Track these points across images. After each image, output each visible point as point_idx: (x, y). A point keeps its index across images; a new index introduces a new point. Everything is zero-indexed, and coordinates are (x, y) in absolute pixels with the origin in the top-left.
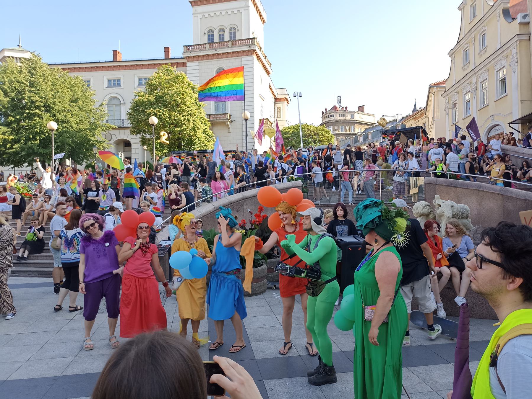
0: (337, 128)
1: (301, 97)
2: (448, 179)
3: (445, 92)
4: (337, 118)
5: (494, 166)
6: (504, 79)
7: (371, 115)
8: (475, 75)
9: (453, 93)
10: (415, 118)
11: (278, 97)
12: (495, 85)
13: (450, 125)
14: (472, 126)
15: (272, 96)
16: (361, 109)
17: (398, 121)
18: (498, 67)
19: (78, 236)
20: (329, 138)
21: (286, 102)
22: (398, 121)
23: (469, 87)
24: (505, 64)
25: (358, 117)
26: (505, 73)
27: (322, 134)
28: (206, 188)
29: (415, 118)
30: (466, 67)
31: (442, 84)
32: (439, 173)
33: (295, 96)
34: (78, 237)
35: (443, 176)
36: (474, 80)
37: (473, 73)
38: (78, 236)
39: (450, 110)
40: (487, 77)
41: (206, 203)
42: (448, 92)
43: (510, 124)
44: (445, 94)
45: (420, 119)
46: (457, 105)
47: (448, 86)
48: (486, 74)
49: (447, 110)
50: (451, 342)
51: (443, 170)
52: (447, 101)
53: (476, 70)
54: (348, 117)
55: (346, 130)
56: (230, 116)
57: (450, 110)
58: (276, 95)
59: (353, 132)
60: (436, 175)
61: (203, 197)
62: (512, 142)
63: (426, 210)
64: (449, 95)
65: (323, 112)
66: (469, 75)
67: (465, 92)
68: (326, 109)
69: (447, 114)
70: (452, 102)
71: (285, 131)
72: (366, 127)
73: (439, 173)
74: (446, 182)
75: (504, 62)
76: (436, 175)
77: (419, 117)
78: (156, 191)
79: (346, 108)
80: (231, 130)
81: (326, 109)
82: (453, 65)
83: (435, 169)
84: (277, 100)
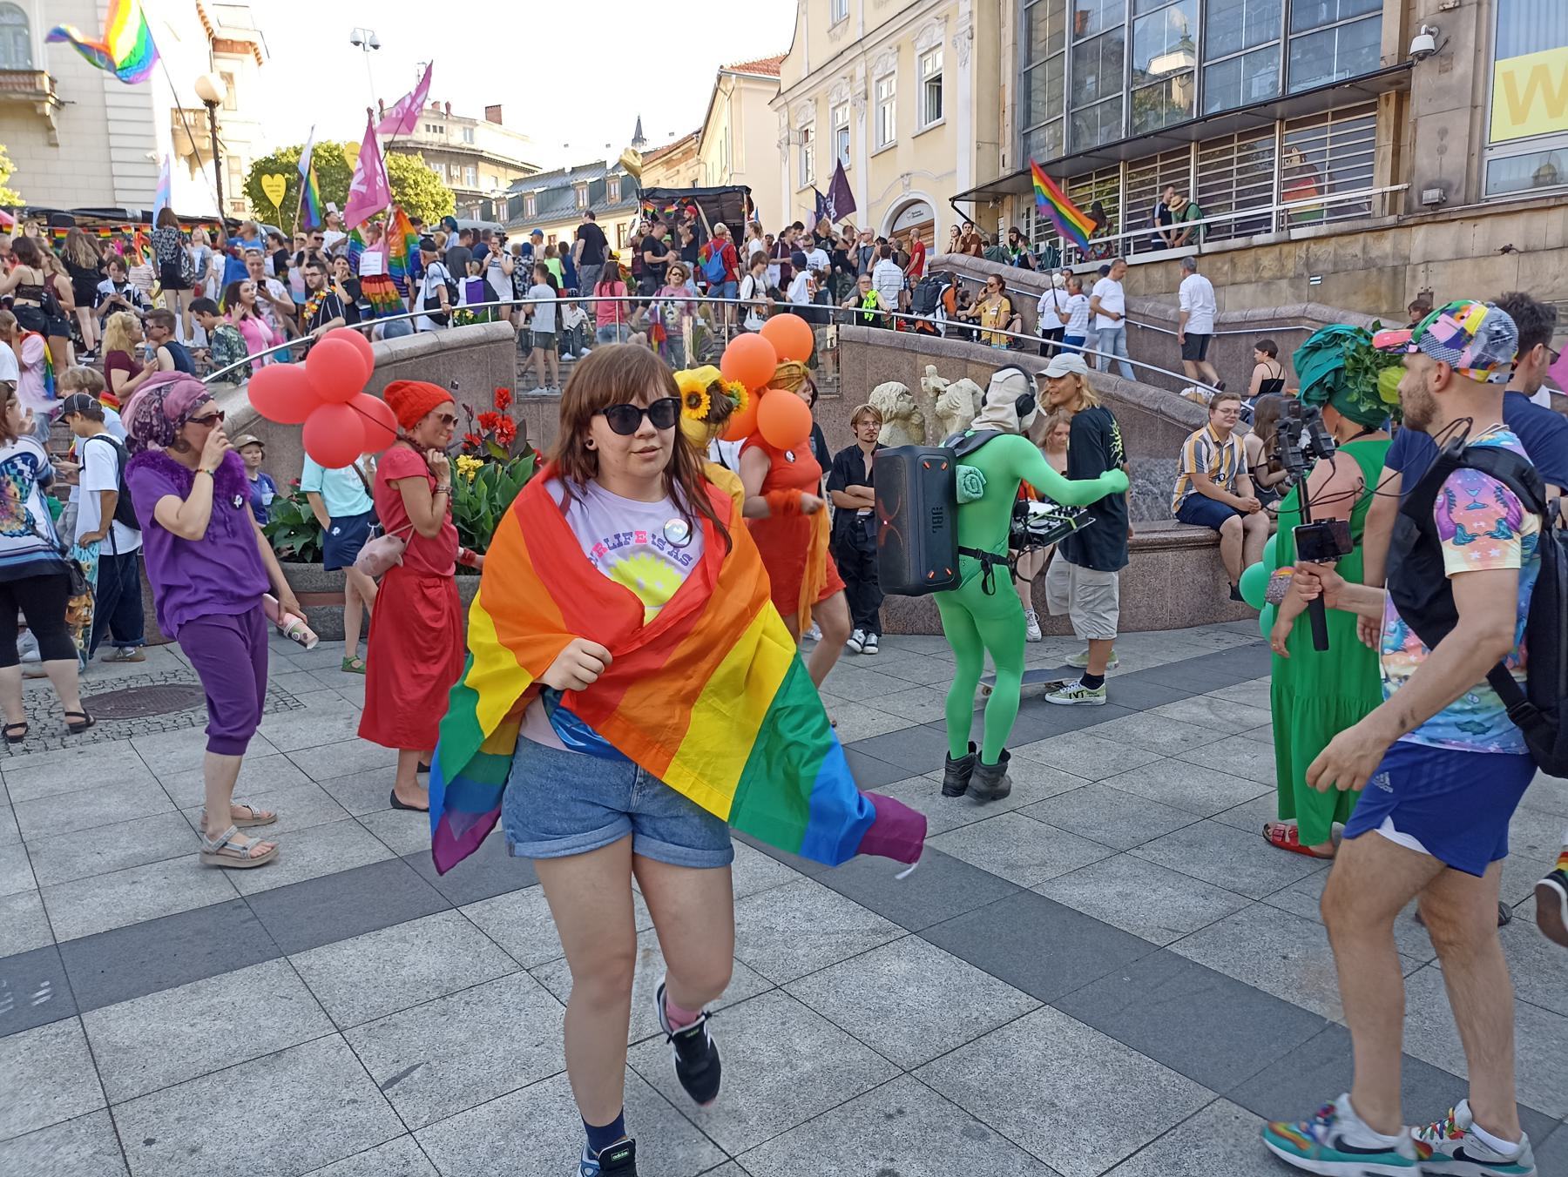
0: (455, 172)
1: (376, 47)
2: (894, 332)
3: (779, 94)
4: (421, 134)
5: (986, 304)
6: (939, 79)
7: (524, 138)
8: (862, 58)
9: (803, 100)
10: (667, 162)
11: (221, 34)
12: (918, 95)
13: (796, 188)
14: (840, 195)
15: (202, 30)
16: (494, 113)
17: (609, 166)
18: (923, 44)
19: (21, 466)
20: (438, 199)
21: (252, 56)
22: (609, 166)
23: (846, 89)
24: (942, 39)
25: (487, 140)
26: (940, 63)
27: (416, 182)
28: (230, 333)
29: (667, 162)
30: (838, 30)
31: (763, 70)
32: (869, 317)
33: (357, 43)
34: (21, 472)
35: (877, 322)
36: (860, 72)
37: (858, 50)
38: (21, 466)
39: (794, 148)
40: (895, 68)
41: (230, 386)
42: (789, 97)
43: (953, 199)
44: (781, 101)
45: (682, 167)
46: (812, 136)
47: (787, 78)
48: (892, 60)
49: (784, 146)
50: (876, 791)
51: (877, 308)
52: (785, 122)
53: (868, 43)
54: (455, 137)
55: (450, 177)
56: (52, 81)
57: (794, 148)
58: (213, 25)
59: (472, 188)
60: (861, 320)
61: (222, 364)
62: (974, 247)
63: (904, 406)
64: (792, 106)
65: (370, 111)
66: (849, 55)
67: (835, 99)
68: (381, 102)
69: (785, 158)
70: (798, 126)
71: (284, 160)
72: (521, 175)
73: (869, 317)
74: (891, 338)
75: (938, 34)
76: (861, 320)
77: (679, 161)
78: (15, 342)
79: (448, 106)
80: (60, 137)
81: (381, 102)
82: (803, 19)
83: (859, 305)
84: (217, 44)
